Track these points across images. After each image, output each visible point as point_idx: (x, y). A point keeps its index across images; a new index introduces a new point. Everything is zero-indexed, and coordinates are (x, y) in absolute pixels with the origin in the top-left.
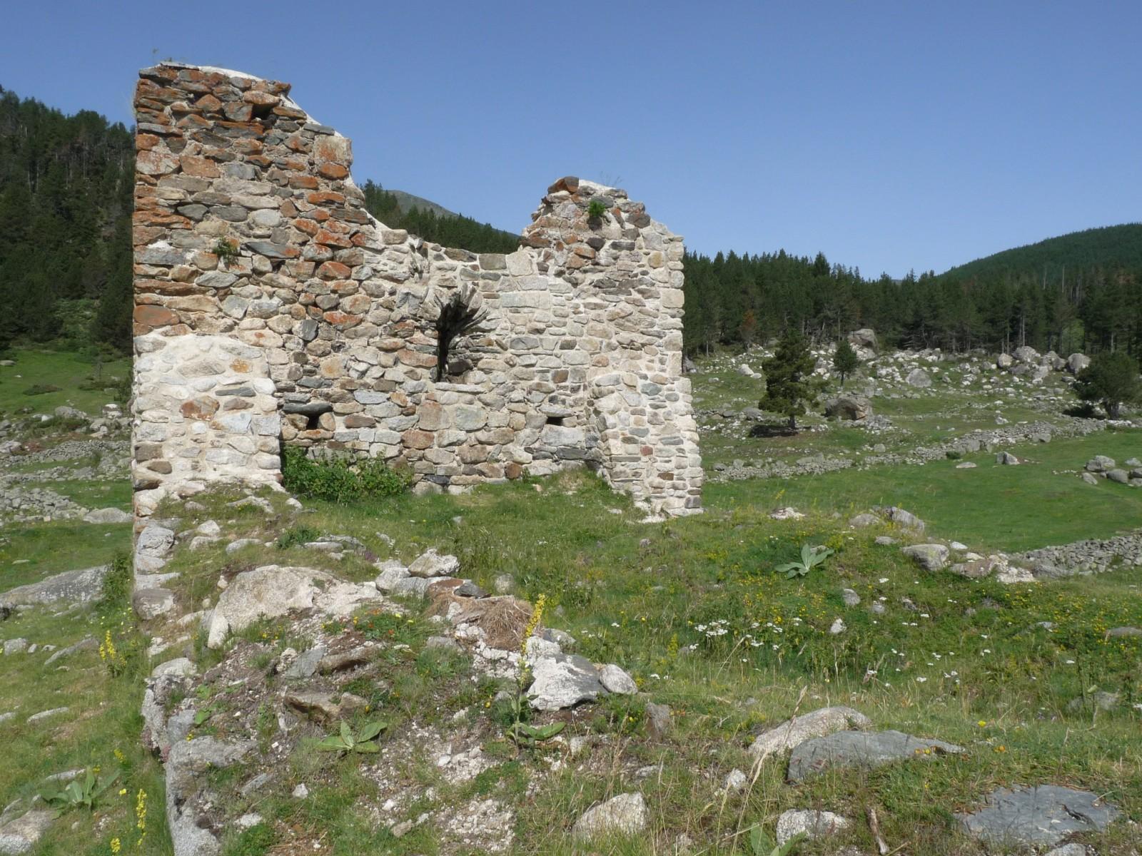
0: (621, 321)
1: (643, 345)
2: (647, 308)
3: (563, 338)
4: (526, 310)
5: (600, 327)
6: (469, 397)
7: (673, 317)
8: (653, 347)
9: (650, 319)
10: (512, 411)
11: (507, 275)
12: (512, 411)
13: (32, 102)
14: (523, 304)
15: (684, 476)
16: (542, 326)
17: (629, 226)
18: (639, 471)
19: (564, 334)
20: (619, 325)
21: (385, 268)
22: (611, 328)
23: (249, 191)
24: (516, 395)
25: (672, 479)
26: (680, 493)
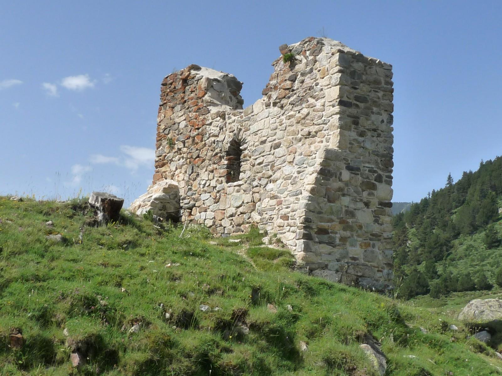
0: (303, 121)
1: (316, 132)
2: (317, 107)
3: (275, 142)
4: (259, 132)
5: (292, 128)
6: (237, 188)
7: (333, 106)
8: (323, 132)
9: (320, 113)
10: (254, 193)
11: (254, 116)
12: (254, 193)
13: (393, 74)
14: (258, 129)
15: (296, 217)
16: (265, 138)
17: (311, 58)
18: (272, 216)
19: (274, 140)
20: (303, 124)
21: (213, 131)
22: (300, 127)
23: (180, 116)
24: (255, 183)
25: (288, 220)
26: (292, 229)
